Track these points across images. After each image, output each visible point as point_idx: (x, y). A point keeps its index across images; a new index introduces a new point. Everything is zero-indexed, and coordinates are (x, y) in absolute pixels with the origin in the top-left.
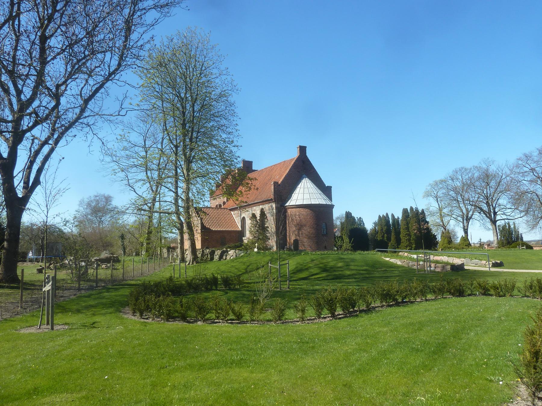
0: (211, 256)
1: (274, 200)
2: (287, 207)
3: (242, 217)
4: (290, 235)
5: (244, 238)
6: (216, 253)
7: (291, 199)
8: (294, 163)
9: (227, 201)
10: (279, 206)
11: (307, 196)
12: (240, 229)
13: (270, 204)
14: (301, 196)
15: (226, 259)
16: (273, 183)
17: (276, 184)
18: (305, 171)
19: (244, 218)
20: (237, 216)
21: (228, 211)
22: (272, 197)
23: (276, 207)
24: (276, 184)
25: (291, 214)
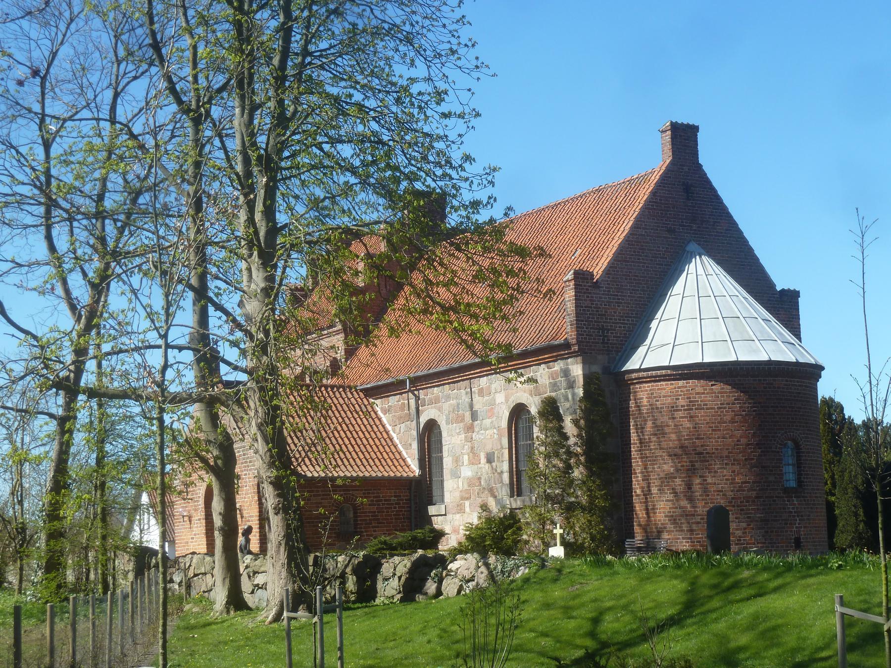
0: (360, 582)
1: (576, 348)
2: (634, 375)
3: (423, 420)
4: (647, 493)
5: (432, 510)
6: (387, 568)
7: (648, 342)
8: (654, 193)
9: (350, 353)
10: (596, 368)
11: (715, 329)
12: (414, 469)
13: (558, 366)
14: (689, 331)
15: (439, 593)
16: (570, 276)
17: (582, 278)
18: (695, 227)
19: (432, 427)
20: (402, 420)
21: (355, 399)
22: (568, 332)
23: (585, 377)
24: (582, 278)
25: (653, 408)
